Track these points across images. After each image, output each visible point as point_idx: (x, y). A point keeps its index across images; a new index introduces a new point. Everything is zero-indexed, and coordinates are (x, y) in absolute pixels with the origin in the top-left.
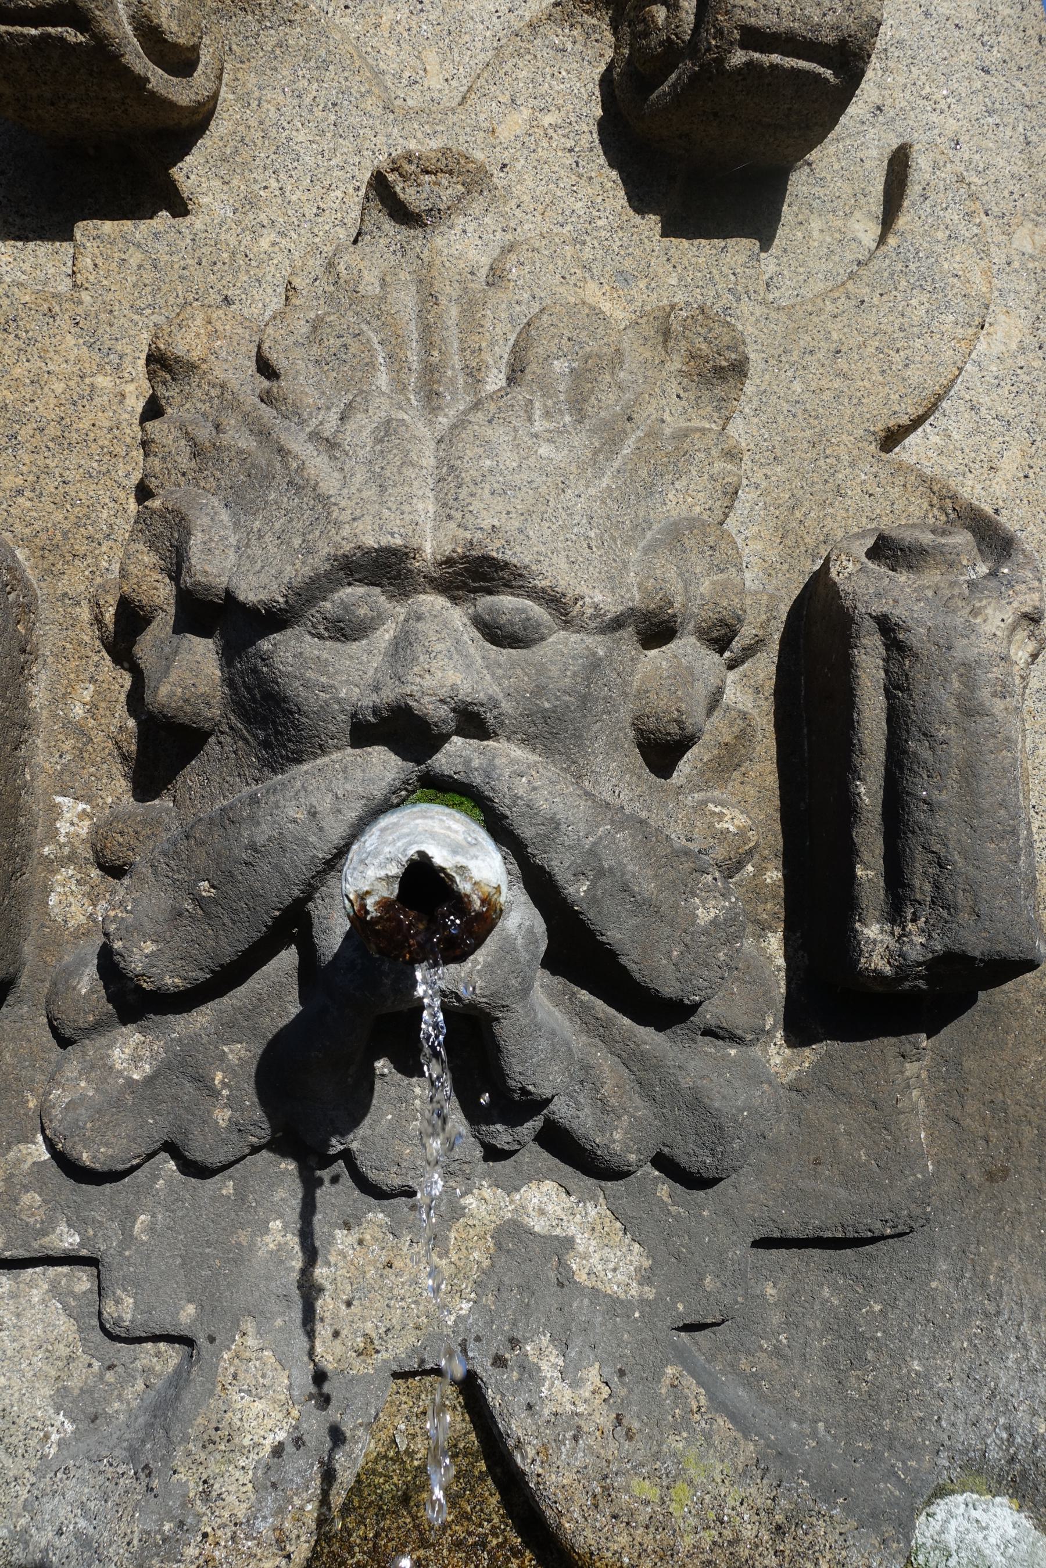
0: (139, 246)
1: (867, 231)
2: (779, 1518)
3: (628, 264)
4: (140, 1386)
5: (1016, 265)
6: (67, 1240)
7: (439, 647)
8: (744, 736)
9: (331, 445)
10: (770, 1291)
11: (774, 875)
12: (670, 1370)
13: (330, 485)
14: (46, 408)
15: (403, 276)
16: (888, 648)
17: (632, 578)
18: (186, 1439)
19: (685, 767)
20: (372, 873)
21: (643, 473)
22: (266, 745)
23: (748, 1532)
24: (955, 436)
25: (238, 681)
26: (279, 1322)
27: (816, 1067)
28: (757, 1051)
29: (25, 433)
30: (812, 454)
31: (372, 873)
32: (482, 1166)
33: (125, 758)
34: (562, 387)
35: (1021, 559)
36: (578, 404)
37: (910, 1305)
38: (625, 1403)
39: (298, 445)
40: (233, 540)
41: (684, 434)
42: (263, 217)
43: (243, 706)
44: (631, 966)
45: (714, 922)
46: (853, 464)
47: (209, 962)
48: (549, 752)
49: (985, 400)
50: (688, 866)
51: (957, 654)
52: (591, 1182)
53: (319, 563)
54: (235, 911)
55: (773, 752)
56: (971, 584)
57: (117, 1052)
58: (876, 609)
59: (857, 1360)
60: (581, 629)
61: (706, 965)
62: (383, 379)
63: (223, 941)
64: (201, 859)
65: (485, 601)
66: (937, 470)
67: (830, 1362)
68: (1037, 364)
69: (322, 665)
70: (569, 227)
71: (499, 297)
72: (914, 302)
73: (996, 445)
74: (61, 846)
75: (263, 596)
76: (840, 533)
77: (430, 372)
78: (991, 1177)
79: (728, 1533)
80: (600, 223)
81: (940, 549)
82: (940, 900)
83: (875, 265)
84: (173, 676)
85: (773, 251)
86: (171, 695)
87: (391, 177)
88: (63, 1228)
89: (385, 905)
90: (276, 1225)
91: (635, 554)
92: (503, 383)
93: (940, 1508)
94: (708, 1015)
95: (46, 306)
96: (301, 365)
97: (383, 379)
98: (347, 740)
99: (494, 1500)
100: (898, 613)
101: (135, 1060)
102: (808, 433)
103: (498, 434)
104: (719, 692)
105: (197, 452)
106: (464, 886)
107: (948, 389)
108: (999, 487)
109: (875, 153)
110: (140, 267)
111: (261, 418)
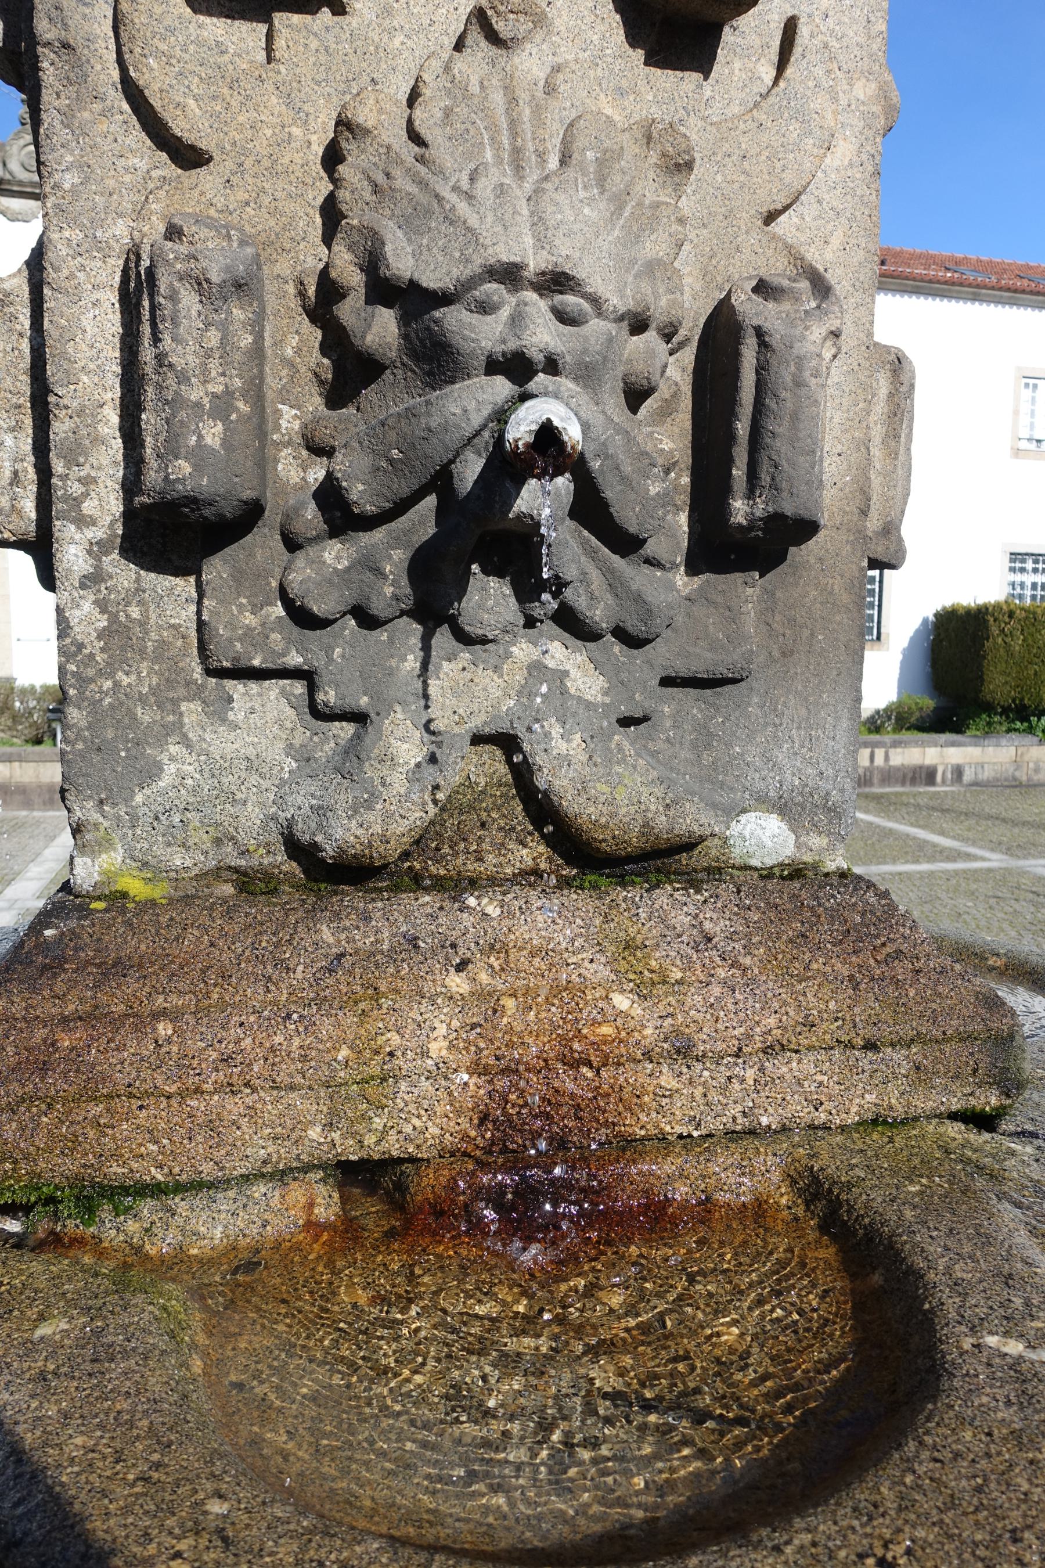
0: (316, 35)
1: (768, 73)
2: (668, 801)
3: (624, 83)
4: (333, 745)
5: (853, 107)
6: (295, 659)
7: (539, 321)
8: (676, 395)
9: (469, 196)
10: (666, 709)
11: (686, 480)
12: (616, 737)
13: (473, 221)
14: (261, 147)
15: (494, 82)
16: (759, 345)
17: (628, 292)
18: (369, 758)
19: (644, 410)
20: (523, 428)
21: (635, 228)
22: (430, 374)
23: (653, 807)
24: (807, 219)
25: (413, 335)
26: (413, 707)
27: (701, 588)
28: (670, 575)
29: (248, 163)
30: (725, 224)
31: (523, 428)
32: (522, 631)
33: (321, 382)
34: (591, 170)
35: (834, 299)
36: (601, 181)
37: (737, 719)
38: (594, 751)
39: (446, 193)
40: (409, 249)
41: (656, 205)
42: (395, 23)
43: (415, 351)
44: (615, 514)
45: (658, 494)
46: (747, 232)
47: (390, 496)
48: (586, 387)
49: (826, 196)
50: (647, 461)
51: (795, 351)
52: (579, 643)
53: (474, 268)
54: (413, 467)
55: (690, 407)
56: (806, 312)
57: (326, 554)
58: (755, 322)
59: (708, 746)
60: (606, 318)
61: (652, 517)
62: (489, 155)
63: (403, 484)
64: (392, 436)
65: (558, 298)
66: (795, 240)
67: (694, 746)
68: (858, 176)
69: (472, 327)
70: (588, 53)
71: (554, 104)
72: (791, 128)
73: (830, 227)
74: (283, 435)
75: (440, 285)
76: (737, 276)
77: (517, 152)
78: (784, 654)
79: (643, 807)
80: (608, 52)
81: (792, 290)
82: (774, 486)
83: (771, 100)
84: (374, 330)
85: (710, 81)
86: (373, 341)
87: (490, 13)
88: (294, 653)
89: (527, 445)
90: (410, 657)
91: (631, 279)
92: (557, 163)
93: (743, 818)
94: (650, 548)
95: (257, 73)
96: (440, 140)
97: (489, 155)
98: (483, 371)
99: (520, 808)
100: (767, 325)
101: (338, 558)
102: (723, 209)
103: (561, 197)
104: (665, 366)
105: (376, 189)
106: (566, 438)
107: (805, 188)
108: (829, 255)
109: (776, 17)
110: (317, 51)
111: (419, 173)
